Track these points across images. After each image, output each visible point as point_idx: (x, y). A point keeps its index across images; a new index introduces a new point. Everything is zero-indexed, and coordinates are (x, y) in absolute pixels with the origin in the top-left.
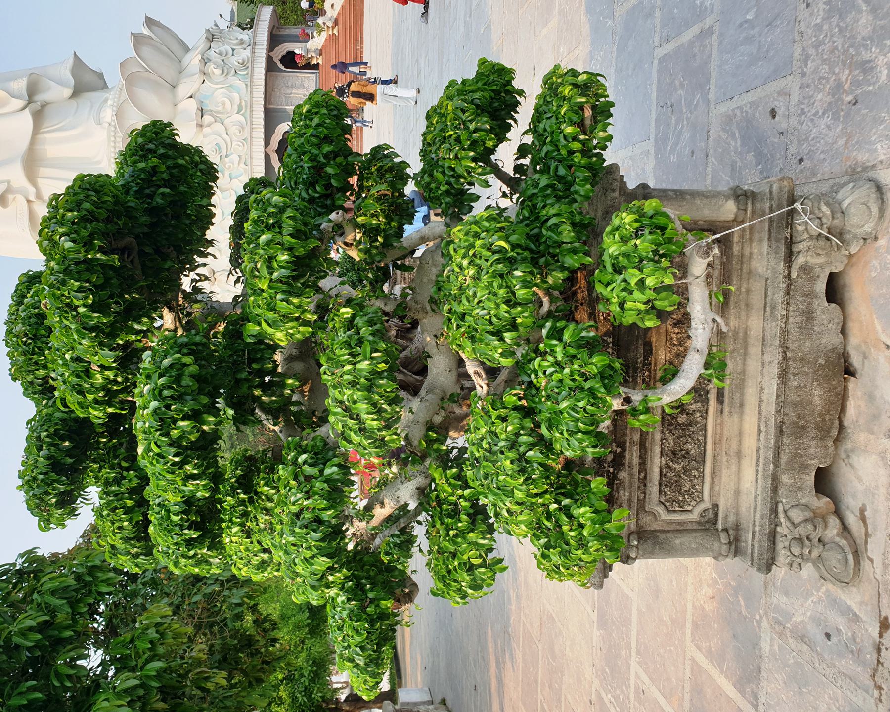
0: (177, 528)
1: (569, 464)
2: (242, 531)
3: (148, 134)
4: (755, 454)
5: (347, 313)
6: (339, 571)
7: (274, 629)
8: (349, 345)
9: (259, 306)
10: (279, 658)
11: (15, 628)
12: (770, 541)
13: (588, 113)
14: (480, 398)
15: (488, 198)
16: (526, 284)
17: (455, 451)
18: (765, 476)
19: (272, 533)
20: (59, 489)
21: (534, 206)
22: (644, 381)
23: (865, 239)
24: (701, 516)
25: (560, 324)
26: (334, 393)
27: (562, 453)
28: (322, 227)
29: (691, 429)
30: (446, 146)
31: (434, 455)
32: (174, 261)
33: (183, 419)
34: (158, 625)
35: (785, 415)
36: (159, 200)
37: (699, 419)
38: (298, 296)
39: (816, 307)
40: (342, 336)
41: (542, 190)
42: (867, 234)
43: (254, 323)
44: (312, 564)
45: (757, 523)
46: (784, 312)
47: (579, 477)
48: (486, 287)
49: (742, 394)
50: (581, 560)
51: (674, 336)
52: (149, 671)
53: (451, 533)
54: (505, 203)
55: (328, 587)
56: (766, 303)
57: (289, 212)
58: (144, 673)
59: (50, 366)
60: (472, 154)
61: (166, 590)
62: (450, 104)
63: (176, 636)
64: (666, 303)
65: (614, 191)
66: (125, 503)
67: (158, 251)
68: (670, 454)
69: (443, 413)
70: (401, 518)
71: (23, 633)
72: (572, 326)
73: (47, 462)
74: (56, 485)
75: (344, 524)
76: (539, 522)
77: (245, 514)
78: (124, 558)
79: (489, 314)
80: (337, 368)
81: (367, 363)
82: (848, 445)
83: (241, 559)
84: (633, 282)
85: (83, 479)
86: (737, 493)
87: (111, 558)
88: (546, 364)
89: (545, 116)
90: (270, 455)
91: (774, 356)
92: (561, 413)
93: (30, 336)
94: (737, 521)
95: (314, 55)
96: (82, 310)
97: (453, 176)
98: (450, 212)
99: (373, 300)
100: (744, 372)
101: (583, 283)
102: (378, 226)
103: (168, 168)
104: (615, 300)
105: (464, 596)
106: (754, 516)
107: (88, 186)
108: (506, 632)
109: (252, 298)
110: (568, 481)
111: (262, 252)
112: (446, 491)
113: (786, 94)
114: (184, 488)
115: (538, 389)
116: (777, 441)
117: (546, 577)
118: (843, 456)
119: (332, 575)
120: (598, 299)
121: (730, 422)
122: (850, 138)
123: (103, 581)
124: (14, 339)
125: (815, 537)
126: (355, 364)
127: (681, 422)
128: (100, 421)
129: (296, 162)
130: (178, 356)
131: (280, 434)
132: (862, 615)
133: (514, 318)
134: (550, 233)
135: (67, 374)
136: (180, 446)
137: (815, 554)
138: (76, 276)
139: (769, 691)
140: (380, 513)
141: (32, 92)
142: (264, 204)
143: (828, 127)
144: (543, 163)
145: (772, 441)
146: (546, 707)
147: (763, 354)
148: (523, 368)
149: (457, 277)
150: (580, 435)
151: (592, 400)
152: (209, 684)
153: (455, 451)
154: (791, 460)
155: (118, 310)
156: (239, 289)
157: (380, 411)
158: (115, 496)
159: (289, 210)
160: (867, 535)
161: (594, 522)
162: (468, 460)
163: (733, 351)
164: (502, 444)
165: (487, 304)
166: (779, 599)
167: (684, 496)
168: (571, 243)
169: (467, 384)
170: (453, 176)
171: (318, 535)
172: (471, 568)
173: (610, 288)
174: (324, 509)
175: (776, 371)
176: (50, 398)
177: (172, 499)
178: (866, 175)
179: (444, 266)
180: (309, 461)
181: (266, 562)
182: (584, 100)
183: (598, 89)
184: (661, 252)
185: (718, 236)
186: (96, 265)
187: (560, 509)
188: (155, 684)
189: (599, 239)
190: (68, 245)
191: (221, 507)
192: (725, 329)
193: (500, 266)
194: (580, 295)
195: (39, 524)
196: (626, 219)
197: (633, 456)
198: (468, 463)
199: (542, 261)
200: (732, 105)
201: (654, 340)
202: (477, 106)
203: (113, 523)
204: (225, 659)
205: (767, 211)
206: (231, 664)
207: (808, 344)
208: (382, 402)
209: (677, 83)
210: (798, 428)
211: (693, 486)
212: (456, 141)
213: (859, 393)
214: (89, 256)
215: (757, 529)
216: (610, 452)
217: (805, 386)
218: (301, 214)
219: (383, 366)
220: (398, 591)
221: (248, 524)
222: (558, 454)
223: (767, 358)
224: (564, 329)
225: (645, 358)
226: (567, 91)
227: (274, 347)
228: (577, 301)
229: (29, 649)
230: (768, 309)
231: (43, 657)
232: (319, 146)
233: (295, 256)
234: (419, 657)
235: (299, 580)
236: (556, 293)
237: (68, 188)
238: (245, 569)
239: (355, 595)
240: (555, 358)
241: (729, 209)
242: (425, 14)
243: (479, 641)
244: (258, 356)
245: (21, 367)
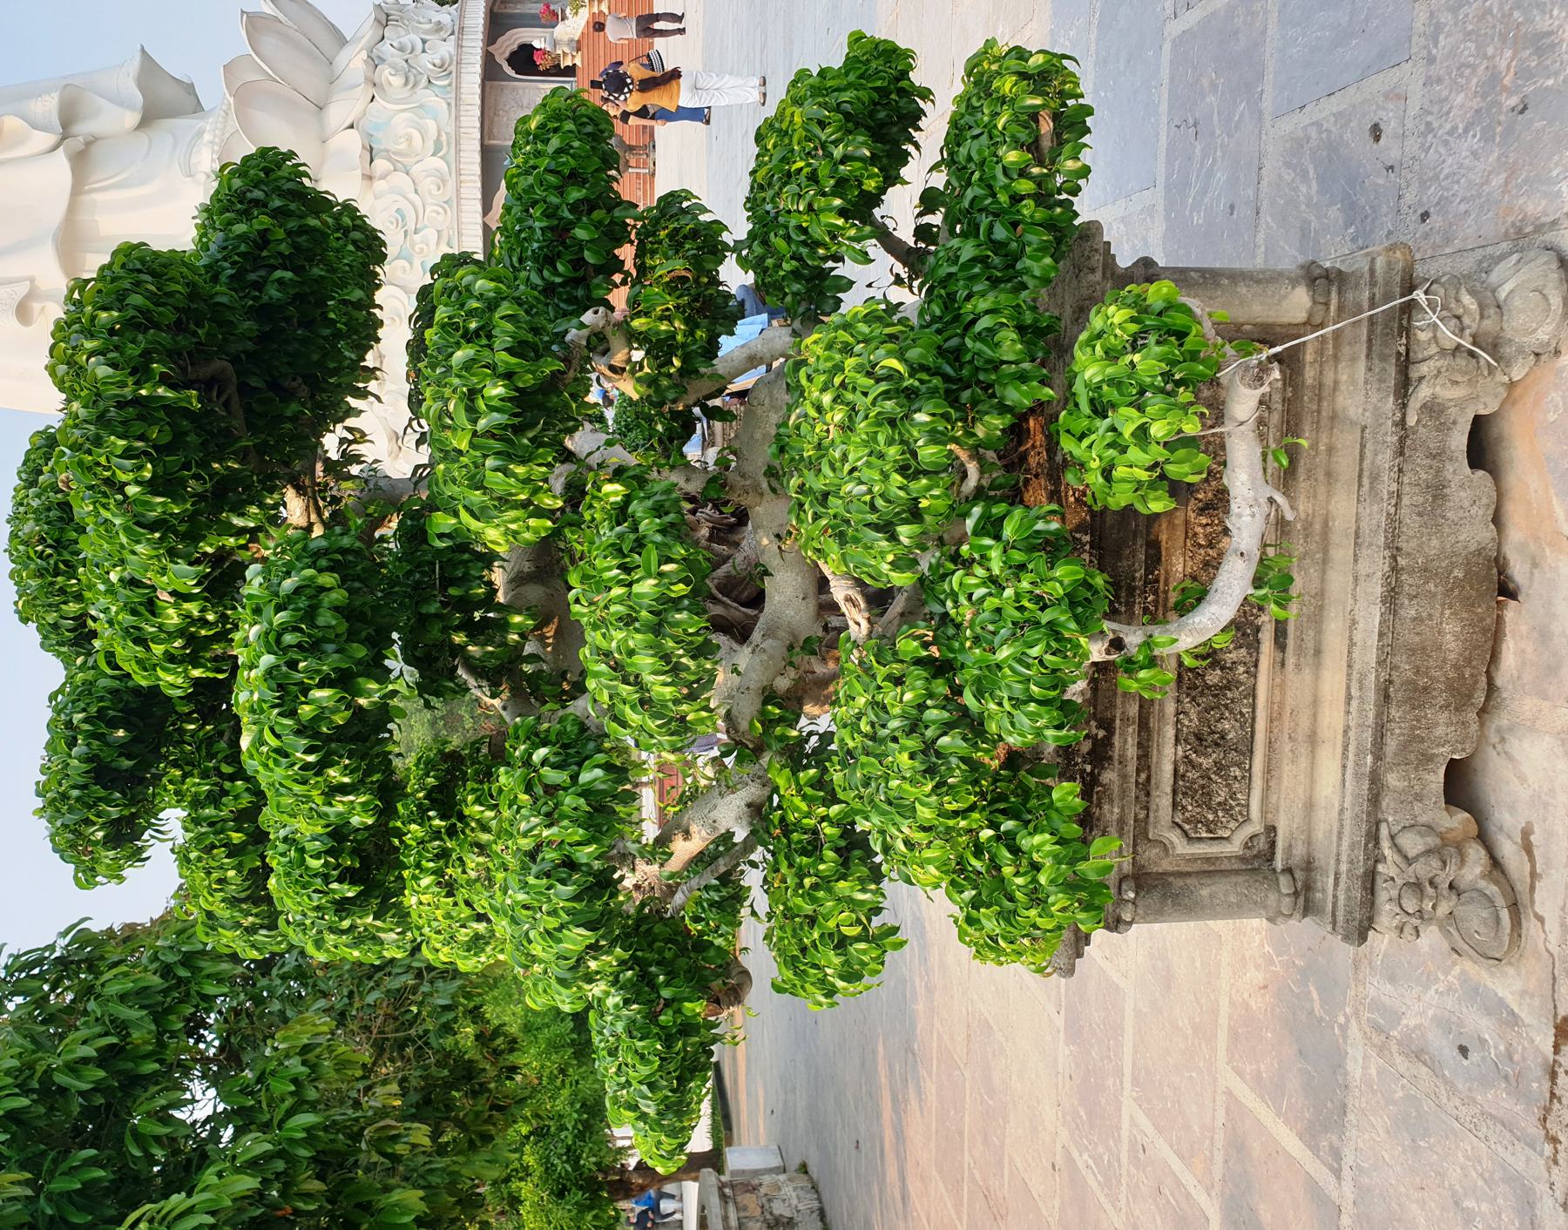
0: (319, 880)
1: (1014, 759)
2: (439, 883)
3: (252, 172)
4: (1340, 737)
5: (616, 493)
6: (608, 953)
7: (512, 1050)
8: (620, 551)
9: (454, 481)
10: (521, 1102)
11: (56, 1063)
12: (1365, 889)
13: (1046, 126)
14: (856, 645)
15: (870, 285)
16: (935, 437)
17: (814, 739)
18: (1358, 776)
19: (491, 886)
20: (108, 814)
21: (951, 297)
22: (1146, 611)
23: (1537, 355)
24: (1246, 847)
25: (999, 509)
26: (594, 637)
27: (1001, 738)
28: (568, 338)
29: (1229, 695)
30: (792, 188)
31: (776, 746)
32: (303, 405)
33: (321, 686)
34: (306, 1049)
35: (1394, 668)
36: (273, 292)
37: (1243, 677)
38: (523, 462)
39: (1449, 477)
40: (607, 534)
41: (965, 267)
42: (1542, 345)
43: (445, 511)
44: (559, 941)
45: (1344, 858)
46: (1394, 487)
47: (1032, 781)
48: (865, 443)
49: (1319, 632)
50: (1035, 926)
51: (1199, 530)
52: (291, 1129)
53: (807, 882)
54: (897, 295)
55: (589, 979)
56: (1361, 470)
57: (506, 309)
58: (284, 1134)
59: (88, 595)
60: (837, 202)
61: (322, 986)
62: (798, 111)
63: (342, 1065)
64: (1186, 468)
65: (1093, 270)
66: (229, 838)
67: (274, 386)
68: (1192, 739)
69: (792, 673)
70: (720, 858)
71: (74, 1068)
72: (1018, 512)
73: (85, 767)
74: (103, 807)
75: (614, 870)
76: (961, 861)
77: (444, 854)
78: (229, 934)
79: (870, 491)
80: (599, 593)
81: (652, 582)
82: (1502, 720)
83: (439, 932)
84: (1127, 430)
85: (154, 795)
86: (1310, 806)
87: (207, 934)
88: (973, 581)
89: (969, 134)
90: (485, 750)
91: (1376, 564)
92: (999, 667)
93: (50, 541)
94: (1309, 855)
95: (567, 50)
96: (132, 490)
97: (804, 243)
98: (801, 310)
99: (666, 472)
100: (1321, 594)
101: (1039, 439)
102: (672, 336)
103: (289, 233)
104: (1095, 465)
105: (831, 992)
106: (1339, 845)
107: (139, 266)
108: (909, 1049)
109: (442, 467)
110: (1011, 788)
111: (456, 381)
112: (797, 809)
113: (1398, 96)
114: (326, 809)
115: (958, 626)
116: (1379, 715)
117: (975, 957)
118: (1494, 738)
119: (595, 959)
120: (1068, 463)
121: (1298, 683)
122: (1513, 173)
123: (208, 976)
124: (21, 548)
125: (1443, 881)
126: (630, 585)
127: (1211, 682)
128: (179, 693)
129: (519, 220)
130: (310, 572)
131: (504, 713)
132: (1523, 1015)
133: (916, 499)
134: (979, 345)
135: (114, 609)
136: (316, 735)
137: (1443, 909)
138: (120, 430)
139: (1361, 1145)
140: (684, 849)
142: (460, 294)
143: (1474, 154)
144: (965, 219)
145: (1371, 715)
146: (978, 1176)
147: (1356, 561)
148: (932, 590)
149: (813, 427)
150: (1032, 707)
151: (1054, 644)
152: (398, 1147)
153: (814, 739)
154: (1404, 747)
155: (200, 489)
156: (424, 455)
157: (676, 669)
158: (211, 824)
159: (505, 304)
160: (1534, 875)
161: (1058, 860)
162: (835, 753)
163: (1302, 558)
164: (894, 724)
165: (867, 474)
166: (1377, 988)
167: (1215, 812)
168: (1016, 363)
169: (835, 621)
170: (804, 243)
171: (570, 889)
172: (842, 943)
173: (1086, 442)
174: (579, 844)
175: (1377, 589)
176: (89, 654)
177: (308, 829)
178: (1540, 239)
179: (790, 408)
180: (552, 759)
181: (483, 937)
182: (1038, 101)
183: (1064, 83)
184: (1177, 377)
185: (1278, 349)
186: (156, 409)
187: (998, 838)
188: (304, 1153)
189: (1067, 358)
190: (103, 371)
191: (402, 842)
192: (1289, 516)
193: (889, 405)
194: (1033, 461)
195: (75, 877)
196: (1114, 317)
197: (1126, 744)
198: (835, 759)
199: (965, 396)
200: (1303, 119)
201: (1163, 537)
202: (847, 115)
203: (209, 873)
204: (428, 1104)
205: (1366, 305)
206: (437, 1109)
207: (1434, 542)
208: (681, 652)
209: (1205, 82)
210: (1415, 690)
211: (1233, 795)
212: (808, 179)
213: (1524, 628)
214: (143, 392)
215: (1344, 867)
216: (1087, 737)
217: (1430, 617)
218: (527, 312)
219: (680, 589)
220: (716, 984)
221: (449, 871)
222: (994, 742)
223: (1363, 568)
224: (1004, 516)
225: (1149, 571)
226: (1007, 85)
227: (488, 559)
228: (1028, 471)
229: (81, 1093)
230: (1366, 481)
231: (108, 1106)
232: (561, 190)
233: (517, 389)
234: (761, 1093)
235: (537, 968)
236: (991, 455)
237: (102, 268)
238: (446, 949)
239: (638, 994)
240: (988, 569)
241: (1297, 303)
243: (863, 1064)
244: (459, 573)
245: (35, 598)
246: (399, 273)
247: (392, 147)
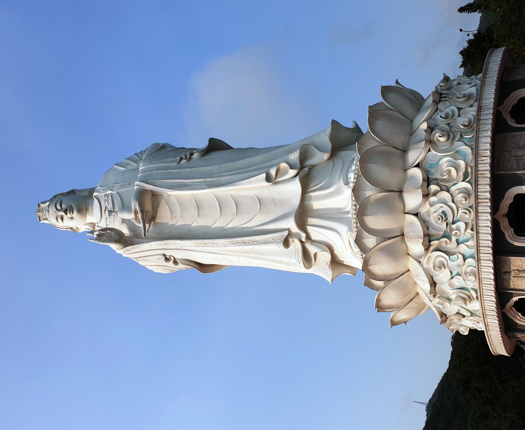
141: (304, 157)
246: (444, 244)
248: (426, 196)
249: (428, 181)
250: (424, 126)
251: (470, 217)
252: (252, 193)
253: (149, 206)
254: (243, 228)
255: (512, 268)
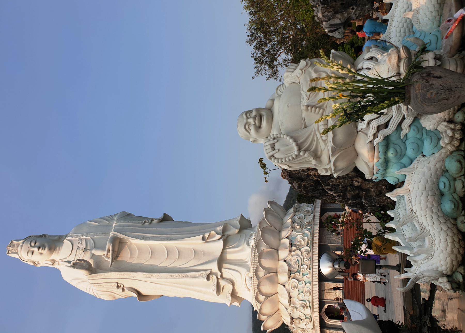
141: (224, 230)
242: (385, 311)
246: (297, 276)
247: (296, 243)
248: (290, 251)
249: (291, 245)
250: (290, 221)
251: (309, 263)
252: (191, 247)
253: (118, 246)
254: (180, 268)
255: (326, 288)
